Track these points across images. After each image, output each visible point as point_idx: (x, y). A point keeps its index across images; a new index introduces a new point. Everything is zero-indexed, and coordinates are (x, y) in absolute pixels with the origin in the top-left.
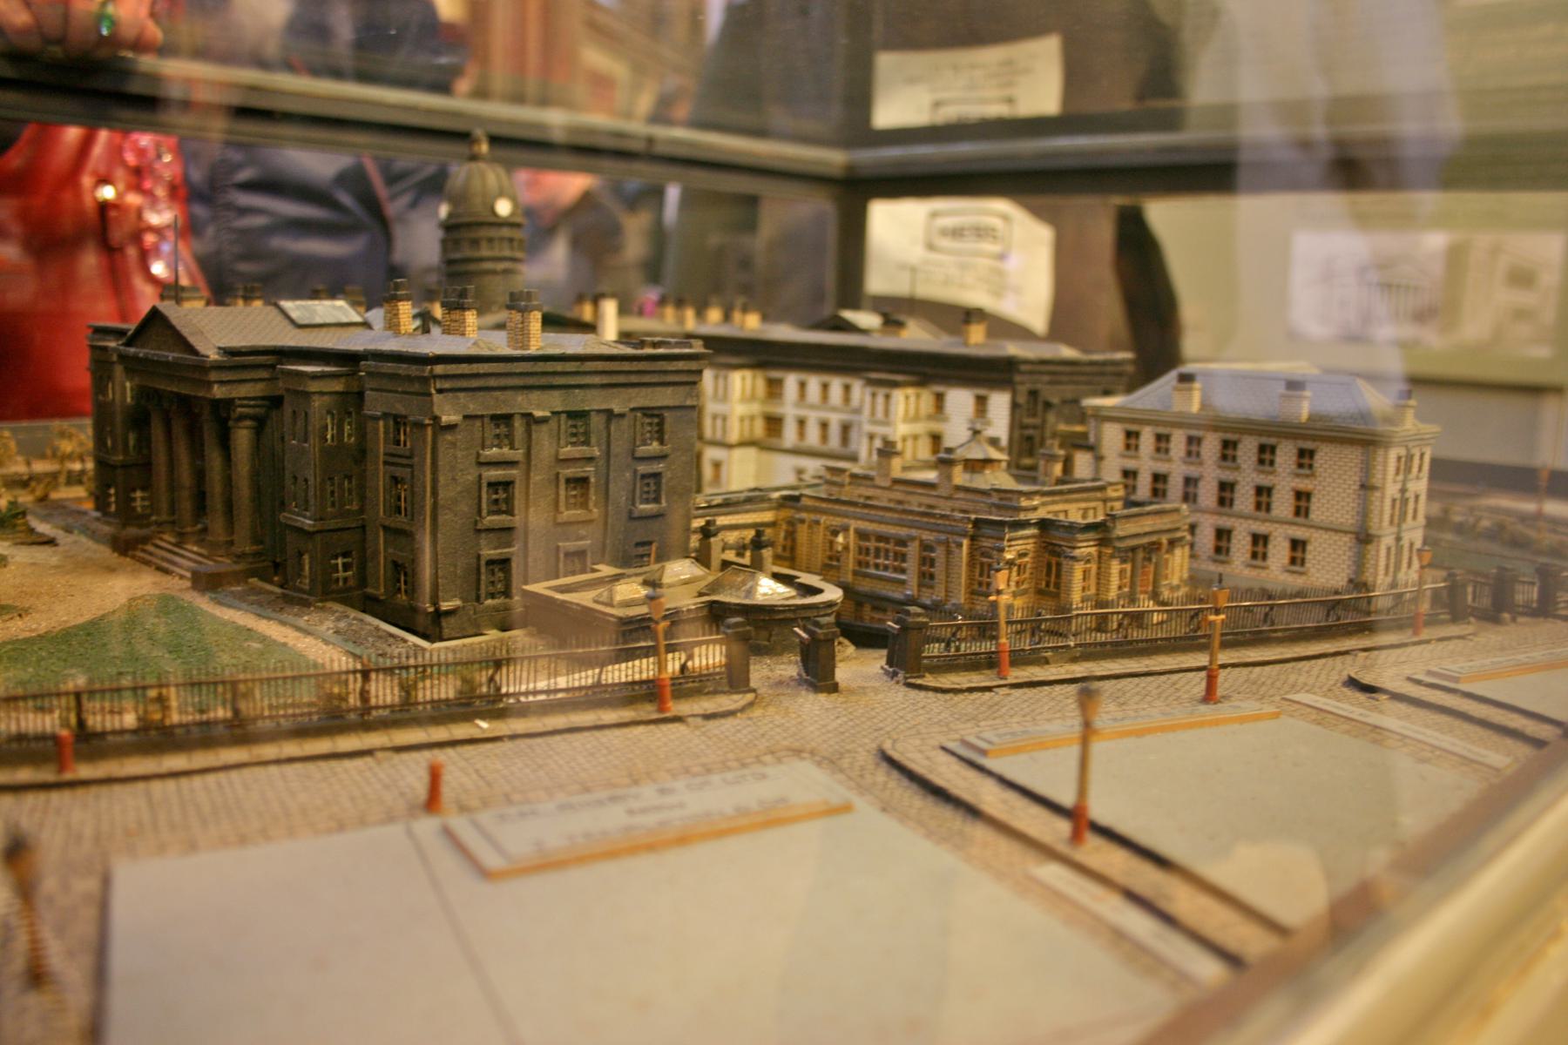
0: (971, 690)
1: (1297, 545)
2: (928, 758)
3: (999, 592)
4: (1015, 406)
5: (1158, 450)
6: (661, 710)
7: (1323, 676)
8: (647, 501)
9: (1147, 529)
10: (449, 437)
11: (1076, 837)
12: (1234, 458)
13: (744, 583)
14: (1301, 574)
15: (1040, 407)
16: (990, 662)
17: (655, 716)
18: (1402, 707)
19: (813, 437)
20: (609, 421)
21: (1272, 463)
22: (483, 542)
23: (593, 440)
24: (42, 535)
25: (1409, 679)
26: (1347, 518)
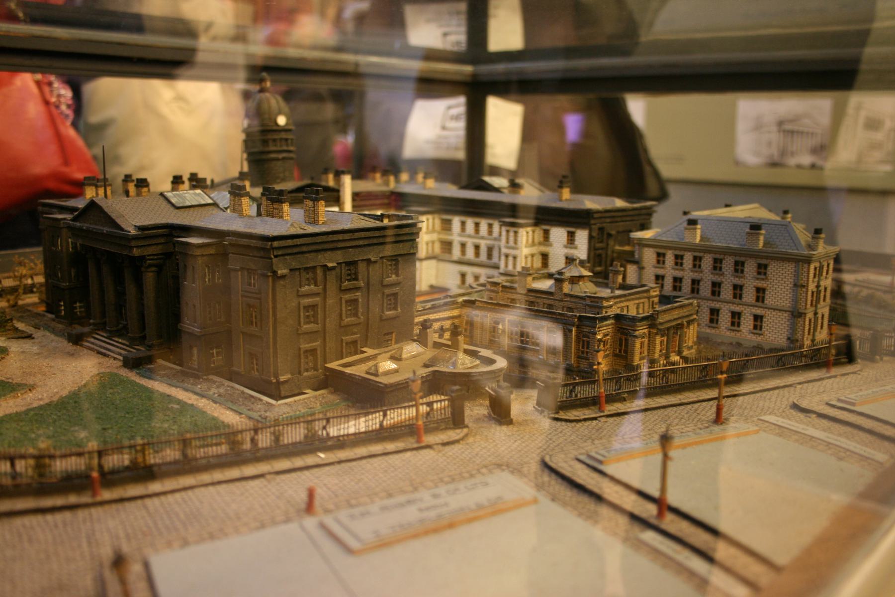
0: (585, 420)
1: (758, 318)
2: (570, 466)
3: (599, 364)
4: (591, 238)
5: (676, 264)
6: (419, 441)
7: (778, 402)
8: (390, 310)
9: (676, 317)
10: (282, 282)
11: (660, 514)
12: (721, 269)
13: (450, 358)
14: (760, 335)
15: (605, 236)
16: (594, 402)
17: (416, 445)
18: (825, 422)
19: (470, 254)
20: (368, 265)
21: (742, 271)
22: (301, 341)
23: (360, 277)
24: (23, 332)
25: (827, 404)
26: (786, 303)
